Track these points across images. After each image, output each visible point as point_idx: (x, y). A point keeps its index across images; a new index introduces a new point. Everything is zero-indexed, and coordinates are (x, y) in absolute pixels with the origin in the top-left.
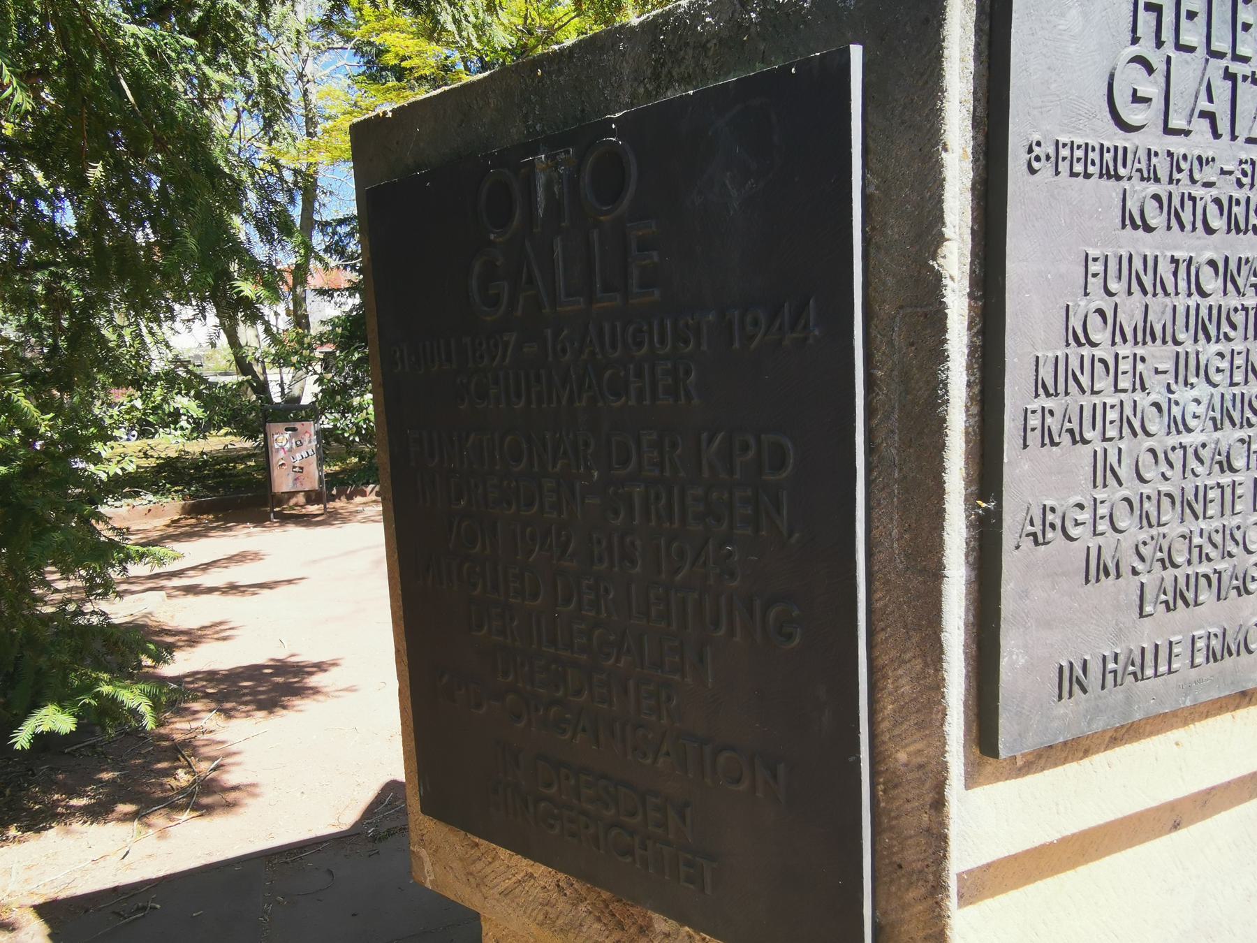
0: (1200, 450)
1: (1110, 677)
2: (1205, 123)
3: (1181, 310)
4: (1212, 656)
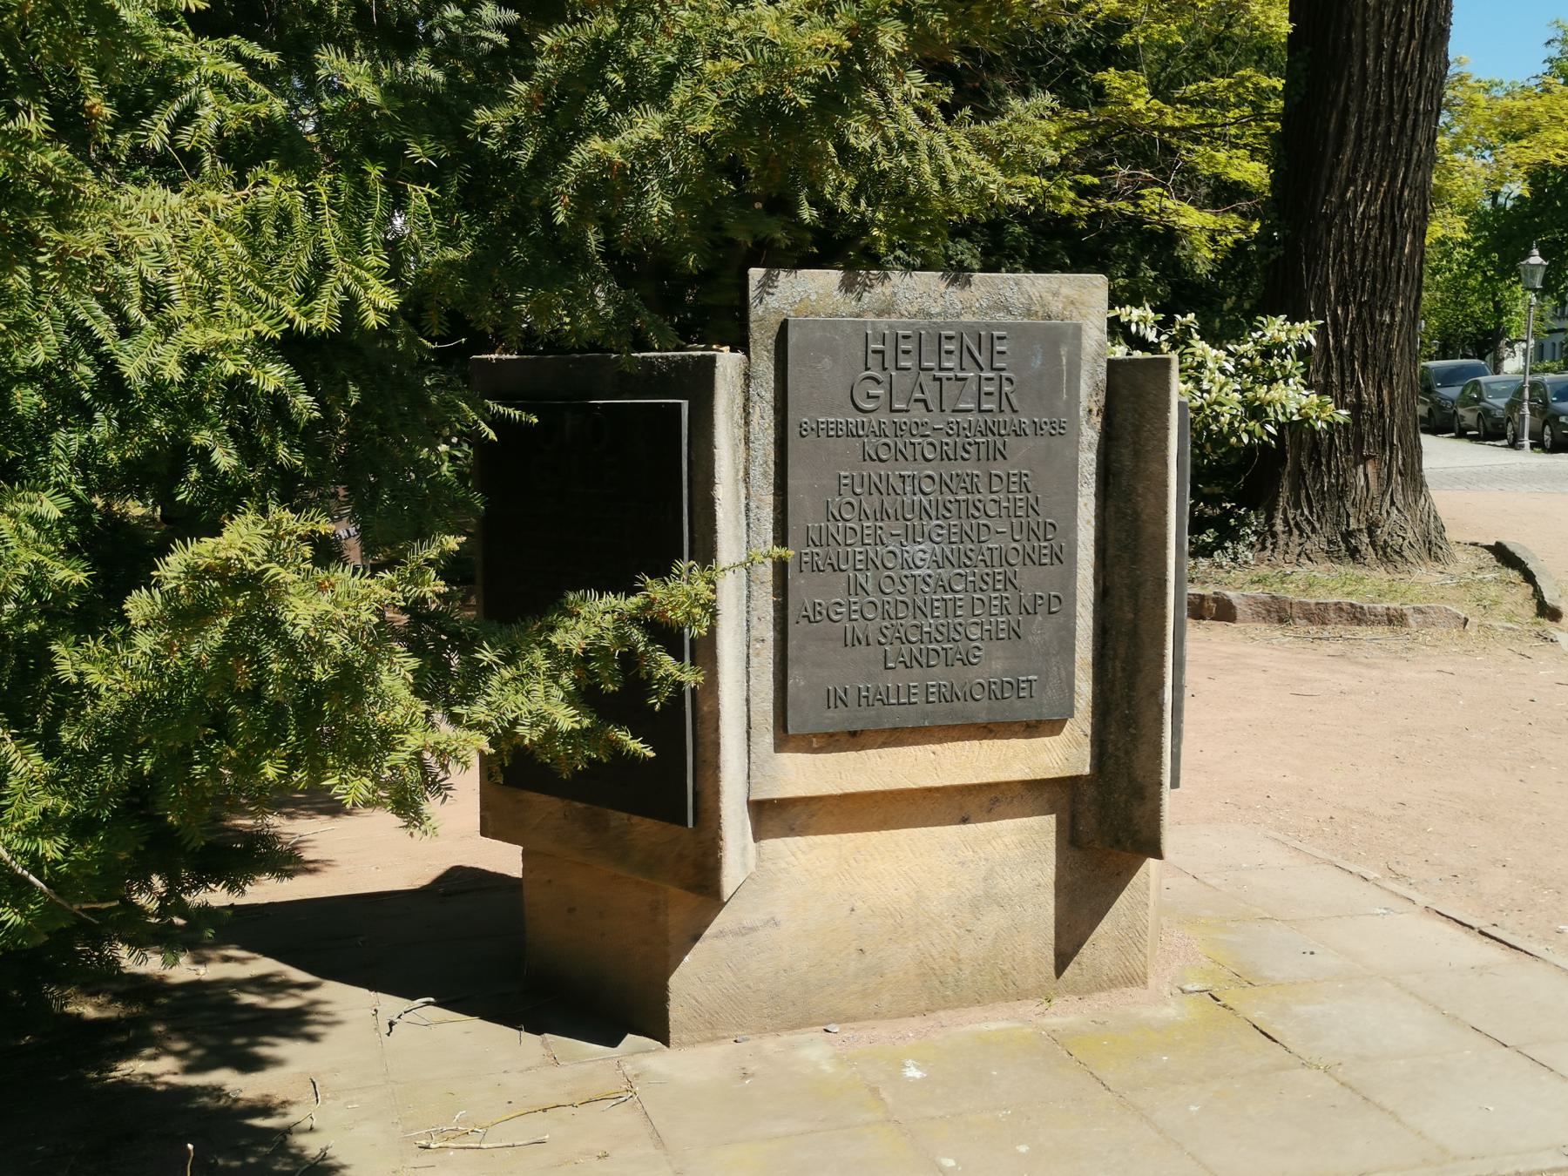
1: (863, 701)
2: (921, 405)
4: (942, 697)
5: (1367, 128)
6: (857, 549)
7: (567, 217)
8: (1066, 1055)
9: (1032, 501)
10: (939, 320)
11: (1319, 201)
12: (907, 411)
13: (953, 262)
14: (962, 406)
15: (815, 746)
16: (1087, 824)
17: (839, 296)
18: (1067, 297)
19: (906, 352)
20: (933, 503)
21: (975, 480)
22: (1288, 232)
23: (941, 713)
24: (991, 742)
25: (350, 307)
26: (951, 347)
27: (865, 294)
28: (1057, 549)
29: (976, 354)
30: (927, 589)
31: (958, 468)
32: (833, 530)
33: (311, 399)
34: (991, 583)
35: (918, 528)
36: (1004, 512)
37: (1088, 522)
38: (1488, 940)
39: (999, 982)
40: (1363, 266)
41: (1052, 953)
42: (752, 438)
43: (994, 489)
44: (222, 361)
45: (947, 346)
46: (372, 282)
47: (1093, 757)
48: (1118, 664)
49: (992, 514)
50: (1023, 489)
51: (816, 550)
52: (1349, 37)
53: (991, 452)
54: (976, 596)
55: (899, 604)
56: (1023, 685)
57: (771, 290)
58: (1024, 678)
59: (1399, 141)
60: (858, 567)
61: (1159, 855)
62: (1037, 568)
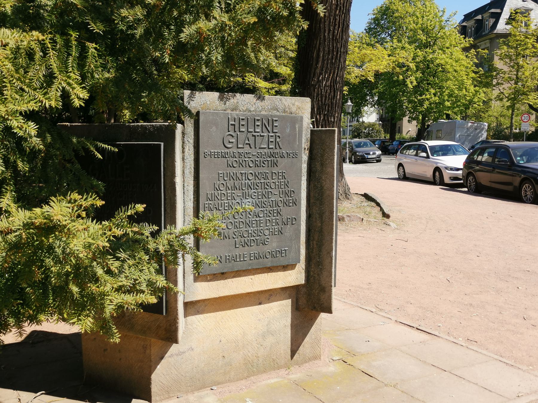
0: (250, 212)
1: (227, 260)
2: (248, 146)
3: (247, 183)
4: (255, 258)
5: (326, 56)
6: (225, 202)
7: (169, 59)
8: (303, 390)
9: (286, 182)
10: (254, 113)
11: (311, 80)
12: (243, 148)
13: (179, 97)
14: (262, 146)
15: (208, 279)
16: (303, 301)
17: (217, 102)
18: (297, 106)
19: (243, 125)
20: (253, 183)
21: (267, 174)
22: (301, 90)
23: (255, 264)
24: (271, 274)
25: (65, 96)
26: (243, 123)
27: (227, 102)
28: (294, 200)
29: (267, 126)
30: (250, 217)
31: (261, 170)
32: (216, 194)
33: (39, 139)
34: (272, 214)
35: (247, 193)
36: (277, 186)
37: (304, 190)
38: (420, 331)
39: (272, 364)
40: (325, 102)
41: (290, 351)
42: (185, 158)
43: (274, 178)
44: (11, 120)
45: (257, 123)
46: (75, 85)
47: (305, 277)
48: (315, 242)
49: (273, 187)
50: (283, 178)
51: (210, 202)
52: (320, 26)
53: (273, 164)
54: (267, 219)
55: (241, 223)
56: (283, 252)
57: (193, 99)
58: (283, 249)
59: (335, 61)
60: (226, 209)
61: (329, 310)
62: (288, 208)
